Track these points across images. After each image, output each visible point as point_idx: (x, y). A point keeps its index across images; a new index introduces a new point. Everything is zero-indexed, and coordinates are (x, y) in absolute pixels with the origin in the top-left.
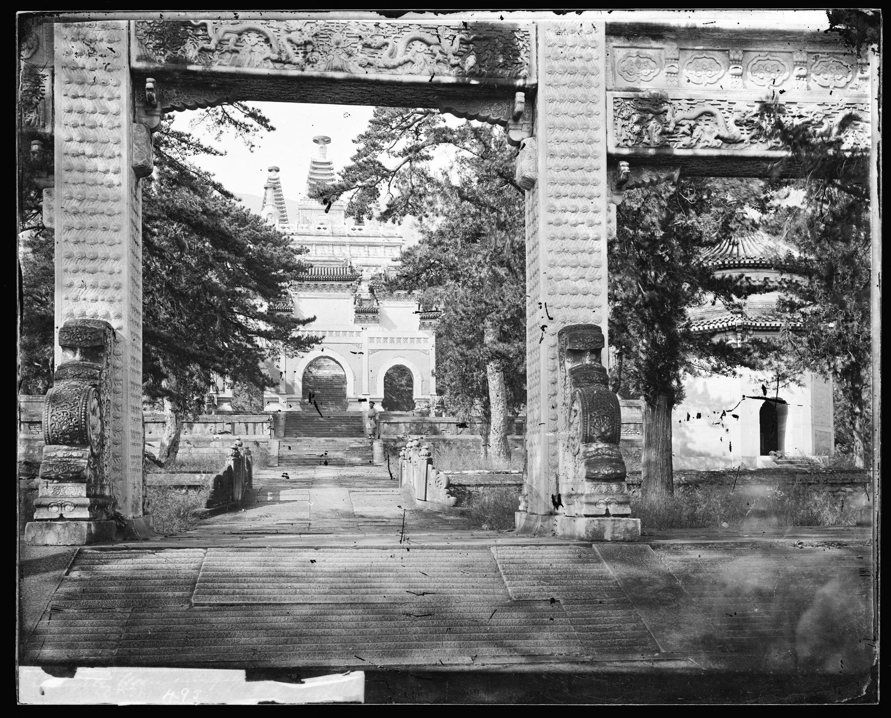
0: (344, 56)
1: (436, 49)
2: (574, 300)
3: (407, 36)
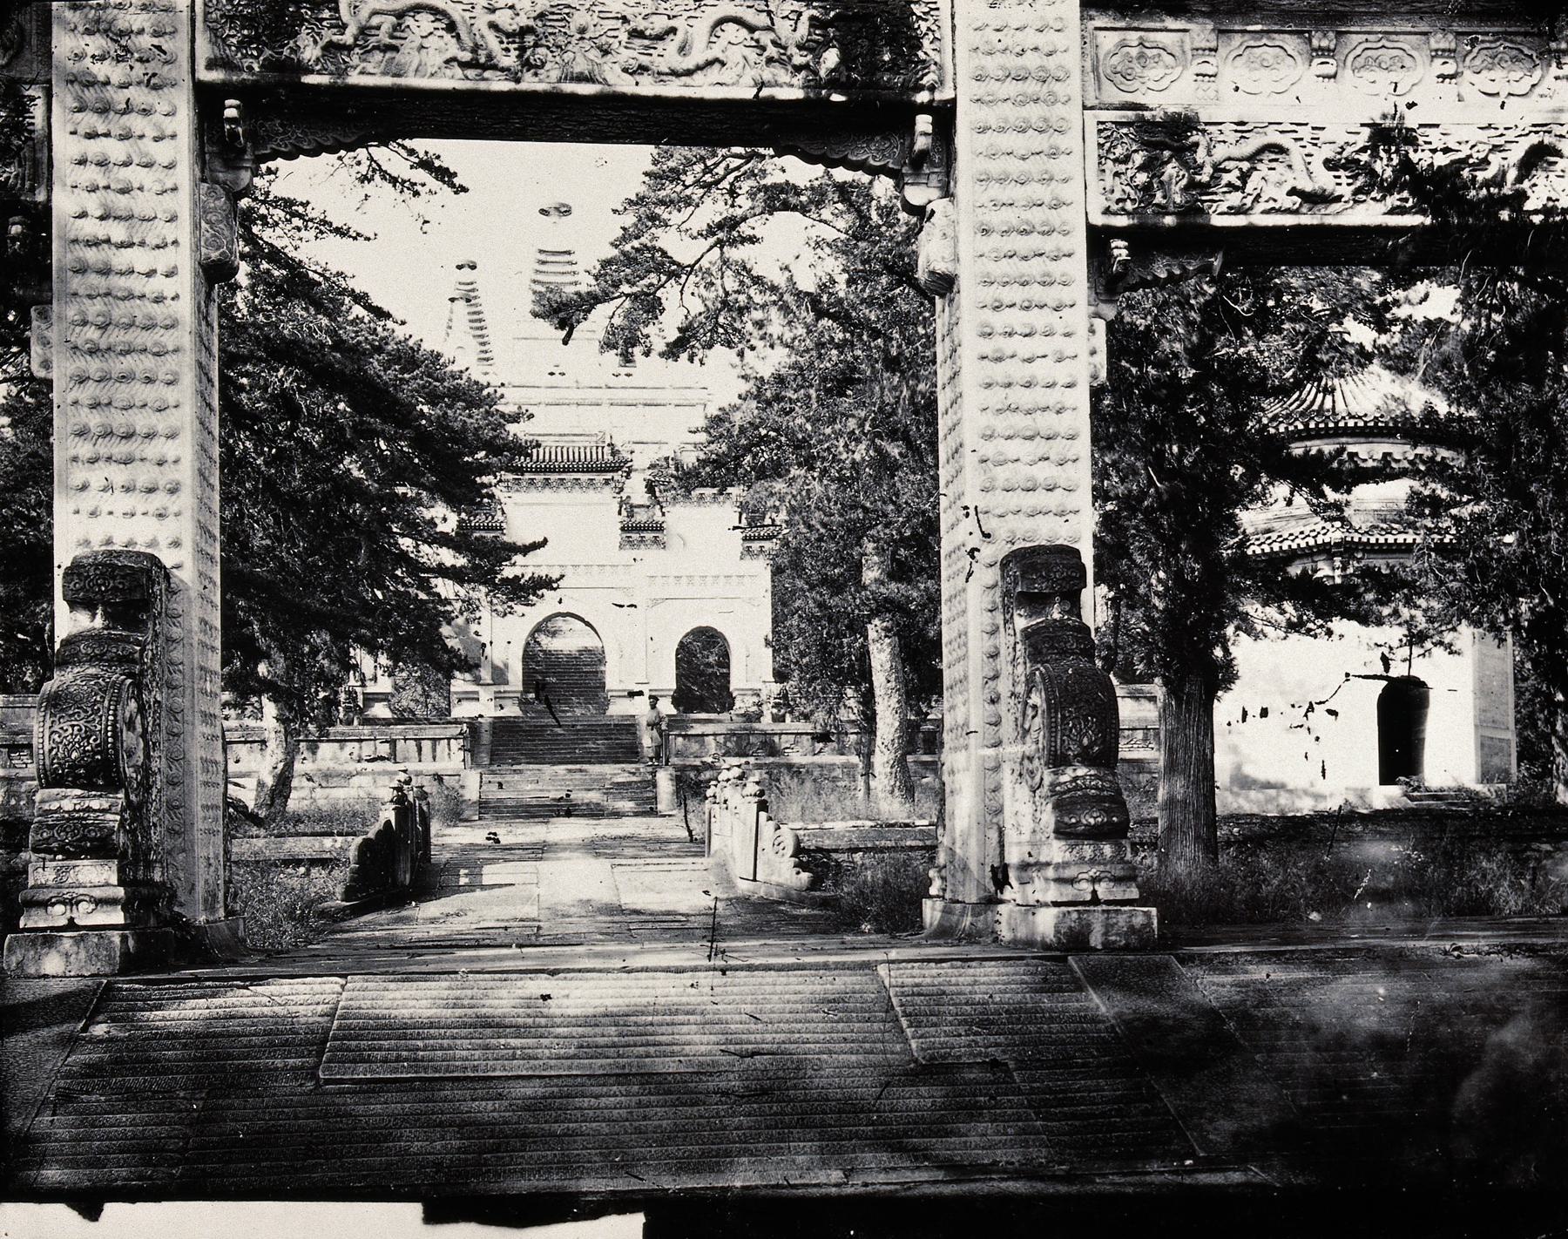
0: (594, 54)
1: (765, 38)
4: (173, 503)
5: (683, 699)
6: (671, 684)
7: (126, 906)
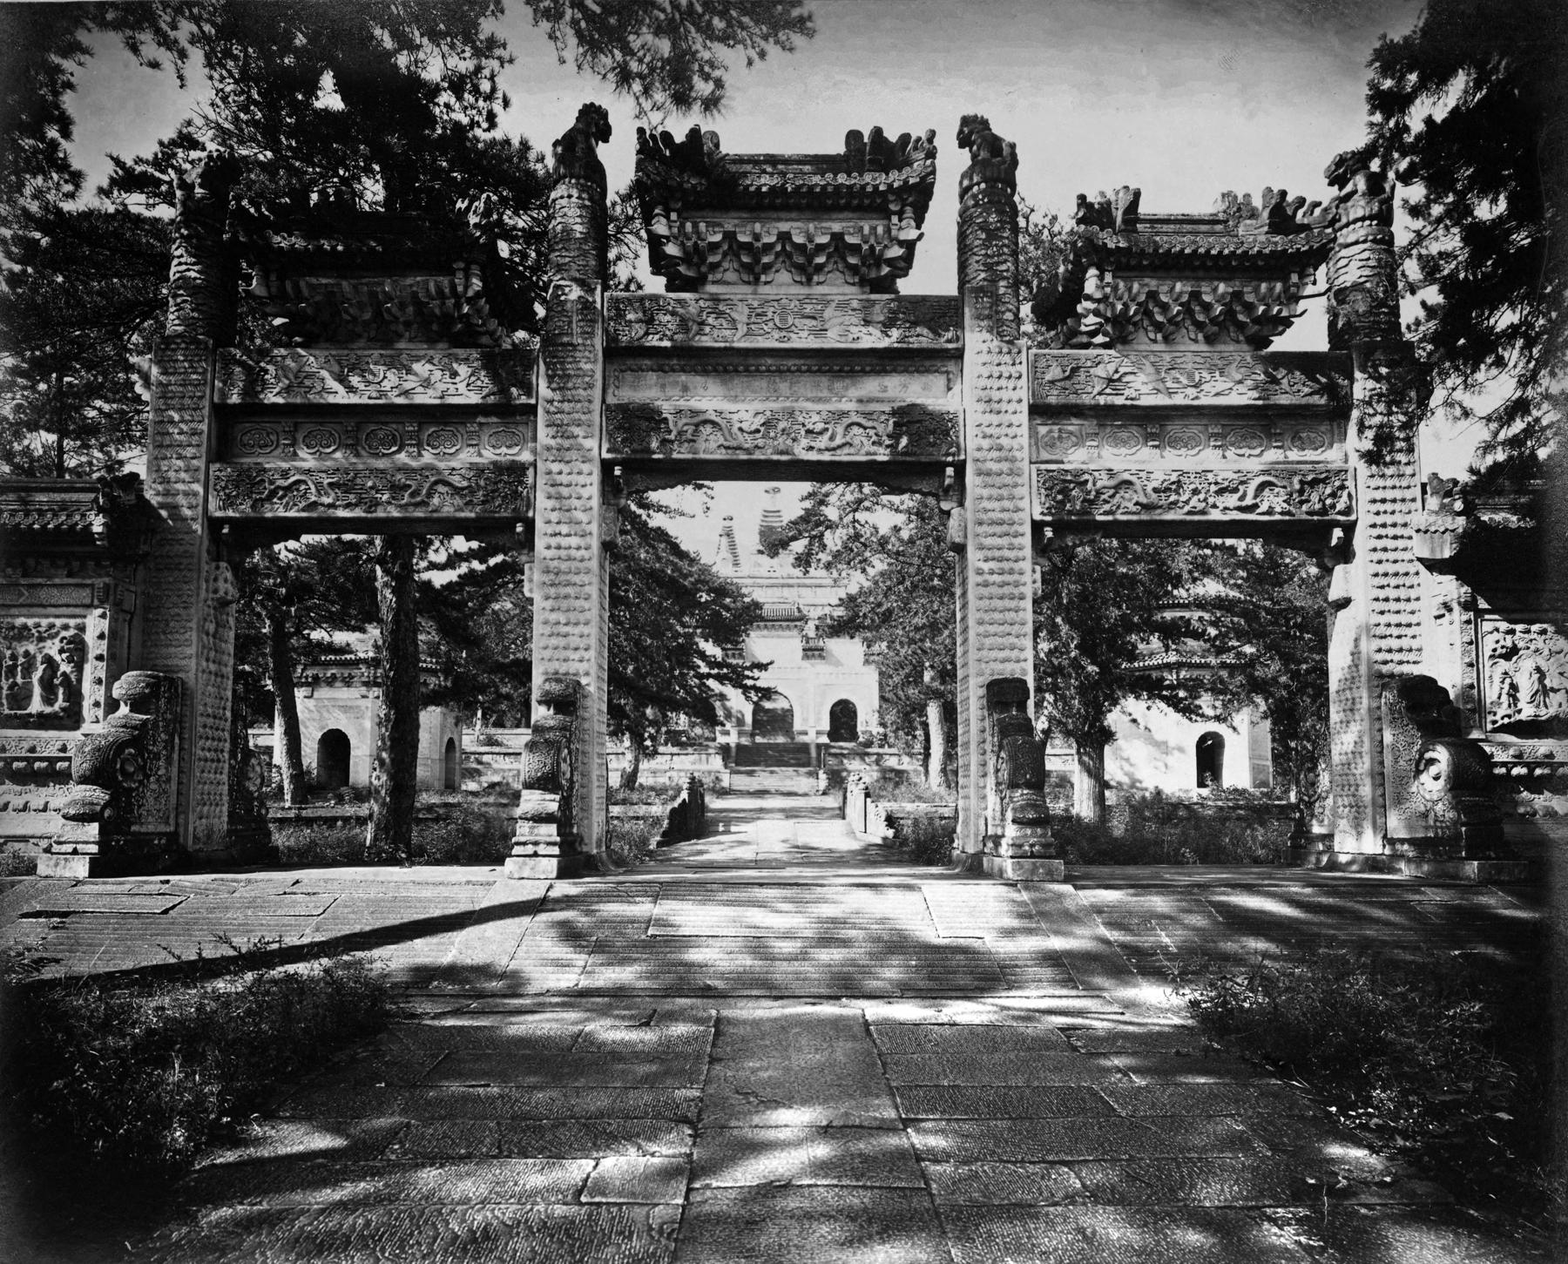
0: (789, 442)
1: (872, 432)
2: (1002, 655)
3: (846, 421)
4: (587, 655)
5: (834, 734)
6: (827, 728)
7: (561, 845)
